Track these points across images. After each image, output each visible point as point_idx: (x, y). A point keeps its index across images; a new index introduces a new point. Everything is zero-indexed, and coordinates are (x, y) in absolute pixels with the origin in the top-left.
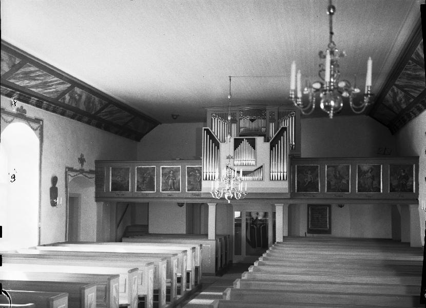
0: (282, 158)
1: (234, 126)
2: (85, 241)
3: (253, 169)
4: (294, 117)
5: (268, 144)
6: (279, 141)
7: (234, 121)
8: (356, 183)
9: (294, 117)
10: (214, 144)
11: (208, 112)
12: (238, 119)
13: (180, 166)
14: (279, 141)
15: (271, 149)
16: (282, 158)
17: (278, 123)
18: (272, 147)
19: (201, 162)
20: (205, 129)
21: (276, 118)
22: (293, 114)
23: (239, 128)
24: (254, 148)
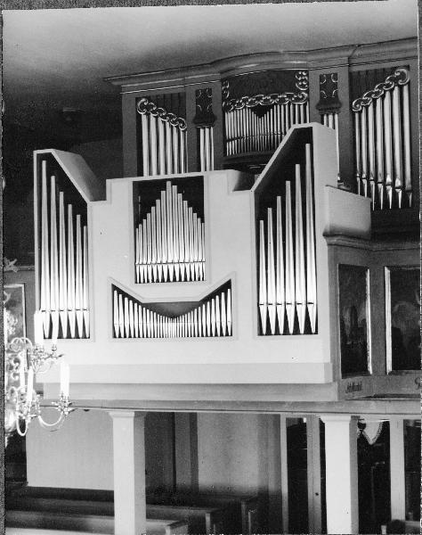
0: (54, 241)
1: (206, 135)
2: (172, 471)
3: (195, 292)
4: (405, 88)
5: (248, 197)
6: (288, 183)
7: (206, 118)
8: (373, 354)
9: (405, 88)
10: (70, 206)
11: (123, 97)
12: (217, 112)
13: (23, 286)
14: (288, 183)
15: (261, 215)
16: (54, 241)
17: (353, 114)
18: (264, 204)
19: (33, 270)
20: (41, 158)
21: (343, 92)
22: (403, 76)
23: (222, 140)
24: (201, 216)
